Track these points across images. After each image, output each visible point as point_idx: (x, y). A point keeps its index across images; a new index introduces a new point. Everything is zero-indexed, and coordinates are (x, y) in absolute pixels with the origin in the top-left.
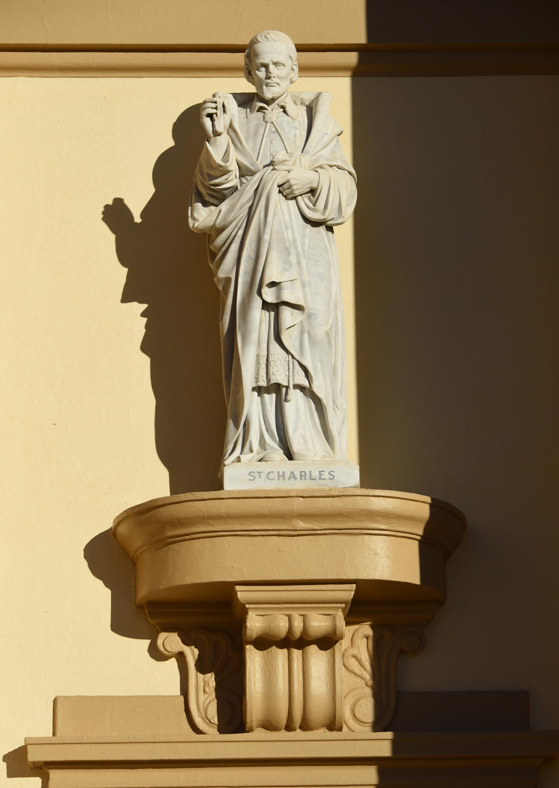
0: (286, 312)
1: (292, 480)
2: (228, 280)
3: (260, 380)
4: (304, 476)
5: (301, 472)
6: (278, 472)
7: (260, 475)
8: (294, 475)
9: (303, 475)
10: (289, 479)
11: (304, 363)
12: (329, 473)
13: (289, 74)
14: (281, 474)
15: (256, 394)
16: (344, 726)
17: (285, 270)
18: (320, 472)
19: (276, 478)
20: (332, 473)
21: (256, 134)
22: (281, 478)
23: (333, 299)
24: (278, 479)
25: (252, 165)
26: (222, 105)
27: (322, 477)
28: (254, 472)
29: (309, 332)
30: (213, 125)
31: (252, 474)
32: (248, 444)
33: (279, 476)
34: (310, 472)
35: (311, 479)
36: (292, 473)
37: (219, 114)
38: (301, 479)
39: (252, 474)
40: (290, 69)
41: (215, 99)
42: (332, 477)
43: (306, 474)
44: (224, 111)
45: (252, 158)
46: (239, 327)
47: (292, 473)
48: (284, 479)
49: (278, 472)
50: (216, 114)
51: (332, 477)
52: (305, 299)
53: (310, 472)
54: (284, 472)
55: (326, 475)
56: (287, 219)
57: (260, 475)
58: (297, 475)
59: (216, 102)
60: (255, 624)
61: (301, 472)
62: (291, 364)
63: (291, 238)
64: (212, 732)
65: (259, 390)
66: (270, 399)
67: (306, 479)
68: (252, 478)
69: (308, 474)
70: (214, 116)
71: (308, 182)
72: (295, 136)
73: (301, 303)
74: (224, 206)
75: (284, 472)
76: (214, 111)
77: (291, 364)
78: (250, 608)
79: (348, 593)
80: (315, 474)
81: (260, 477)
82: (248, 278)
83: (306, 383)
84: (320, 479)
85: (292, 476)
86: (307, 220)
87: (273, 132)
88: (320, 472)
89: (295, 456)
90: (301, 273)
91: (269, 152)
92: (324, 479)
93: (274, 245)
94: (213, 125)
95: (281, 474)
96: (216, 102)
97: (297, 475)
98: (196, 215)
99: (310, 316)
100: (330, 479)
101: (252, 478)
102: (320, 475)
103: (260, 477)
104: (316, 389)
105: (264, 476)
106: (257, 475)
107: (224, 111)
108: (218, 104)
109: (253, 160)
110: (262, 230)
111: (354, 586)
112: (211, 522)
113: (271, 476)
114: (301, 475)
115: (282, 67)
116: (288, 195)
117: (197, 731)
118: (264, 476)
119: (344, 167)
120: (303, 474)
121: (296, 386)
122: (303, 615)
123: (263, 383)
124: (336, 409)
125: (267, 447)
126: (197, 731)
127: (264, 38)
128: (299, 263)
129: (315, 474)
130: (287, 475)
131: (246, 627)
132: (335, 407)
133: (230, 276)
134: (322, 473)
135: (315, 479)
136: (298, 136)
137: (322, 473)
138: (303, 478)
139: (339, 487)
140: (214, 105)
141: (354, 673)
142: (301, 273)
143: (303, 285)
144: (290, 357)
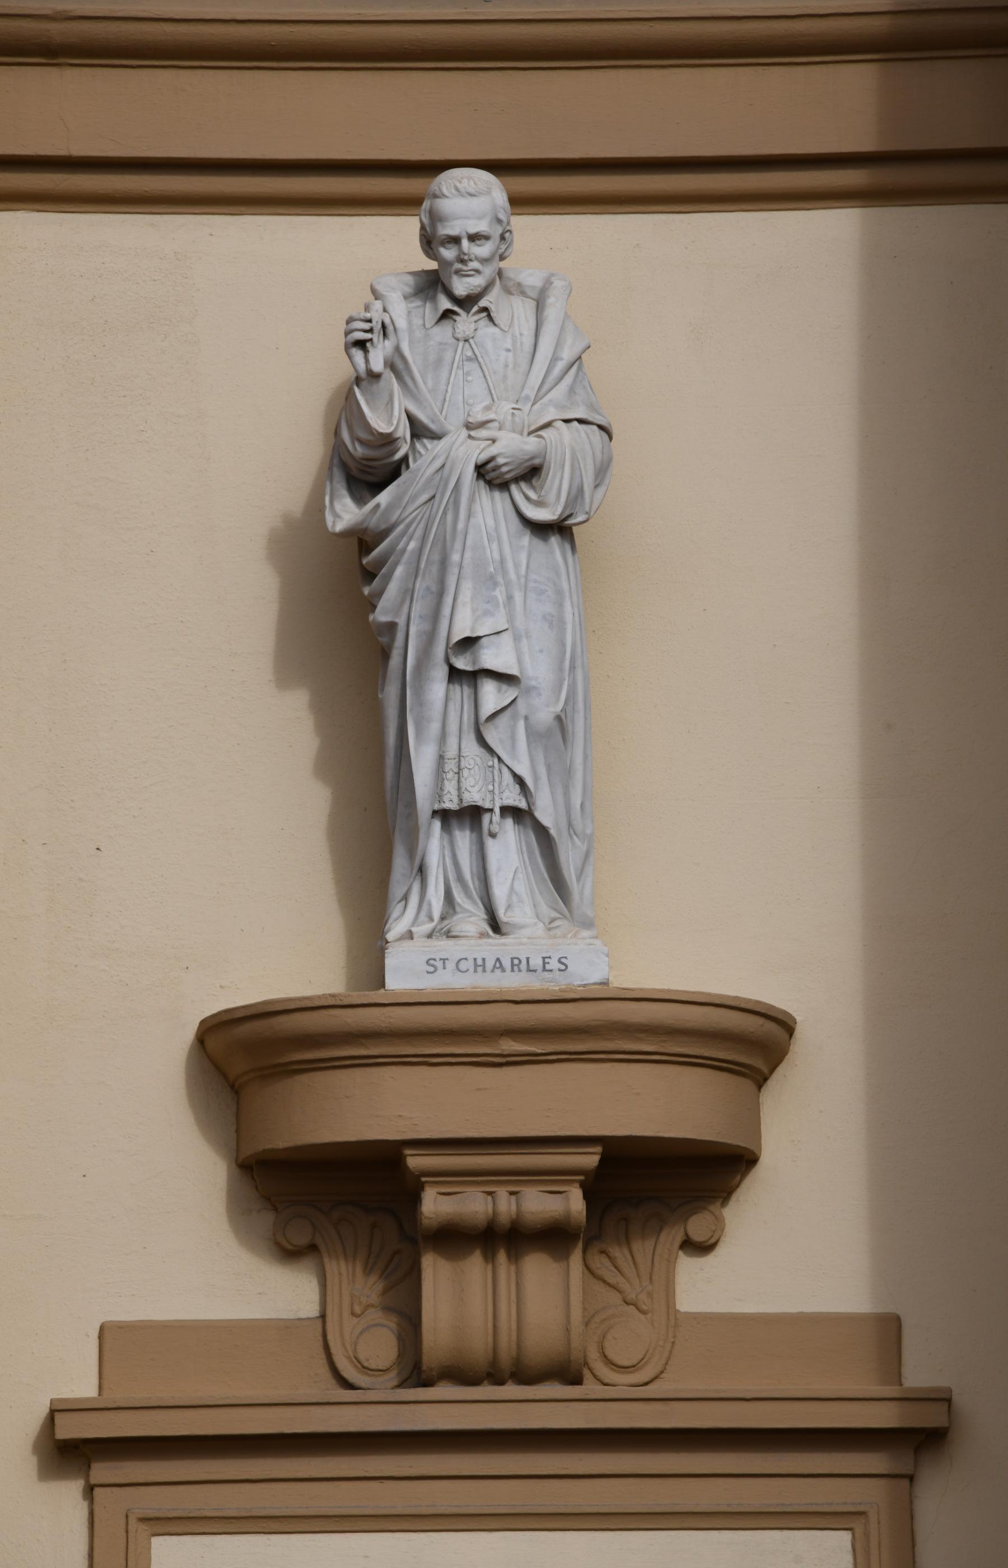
0: (489, 689)
1: (498, 972)
2: (392, 626)
3: (446, 798)
4: (518, 965)
5: (512, 959)
6: (475, 959)
7: (444, 963)
8: (501, 964)
9: (515, 964)
10: (493, 971)
11: (519, 771)
12: (559, 961)
13: (498, 248)
14: (480, 962)
15: (437, 824)
16: (586, 1372)
17: (487, 613)
18: (544, 958)
19: (472, 969)
20: (563, 960)
21: (439, 362)
22: (480, 969)
23: (568, 655)
24: (475, 971)
25: (433, 422)
26: (380, 326)
27: (548, 967)
28: (435, 960)
29: (526, 718)
30: (367, 361)
31: (432, 962)
32: (425, 907)
33: (476, 966)
34: (528, 959)
35: (529, 970)
36: (498, 960)
37: (375, 340)
38: (513, 970)
39: (432, 962)
40: (498, 239)
41: (368, 315)
42: (563, 967)
43: (520, 961)
44: (385, 335)
45: (432, 409)
46: (411, 710)
47: (498, 960)
48: (484, 971)
49: (475, 959)
50: (371, 340)
51: (563, 967)
52: (520, 662)
53: (528, 959)
54: (484, 960)
55: (553, 964)
56: (491, 522)
57: (444, 963)
58: (507, 963)
59: (370, 321)
60: (435, 1205)
61: (512, 959)
62: (496, 772)
63: (496, 556)
64: (384, 1388)
65: (445, 816)
66: (463, 839)
67: (520, 971)
68: (432, 969)
69: (524, 962)
70: (368, 345)
71: (526, 457)
72: (506, 366)
73: (514, 671)
74: (384, 498)
75: (484, 960)
76: (368, 336)
77: (496, 772)
78: (426, 1182)
79: (590, 1159)
80: (536, 962)
81: (444, 968)
82: (426, 626)
83: (523, 805)
84: (544, 969)
85: (498, 965)
86: (528, 523)
87: (469, 359)
88: (544, 958)
89: (504, 930)
90: (511, 618)
91: (461, 397)
92: (551, 971)
93: (467, 570)
94: (367, 361)
95: (480, 962)
96: (370, 321)
97: (507, 963)
98: (338, 507)
99: (553, 275)
100: (560, 970)
101: (432, 969)
102: (544, 963)
103: (444, 968)
104: (539, 815)
105: (451, 965)
106: (439, 964)
107: (385, 335)
108: (374, 322)
109: (435, 414)
110: (448, 544)
111: (599, 1149)
112: (363, 1041)
113: (463, 966)
114: (513, 965)
115: (483, 241)
116: (493, 479)
117: (347, 1385)
118: (451, 965)
119: (590, 419)
120: (516, 962)
121: (505, 810)
122: (512, 1193)
123: (450, 803)
124: (575, 838)
125: (458, 909)
126: (347, 1385)
127: (453, 191)
128: (510, 598)
129: (536, 962)
130: (489, 964)
131: (421, 1213)
132: (572, 833)
133: (397, 620)
134: (547, 960)
135: (535, 971)
136: (511, 366)
137: (547, 960)
138: (516, 968)
139: (576, 983)
140: (366, 326)
141: (605, 1282)
142: (511, 618)
143: (517, 639)
144: (496, 760)
